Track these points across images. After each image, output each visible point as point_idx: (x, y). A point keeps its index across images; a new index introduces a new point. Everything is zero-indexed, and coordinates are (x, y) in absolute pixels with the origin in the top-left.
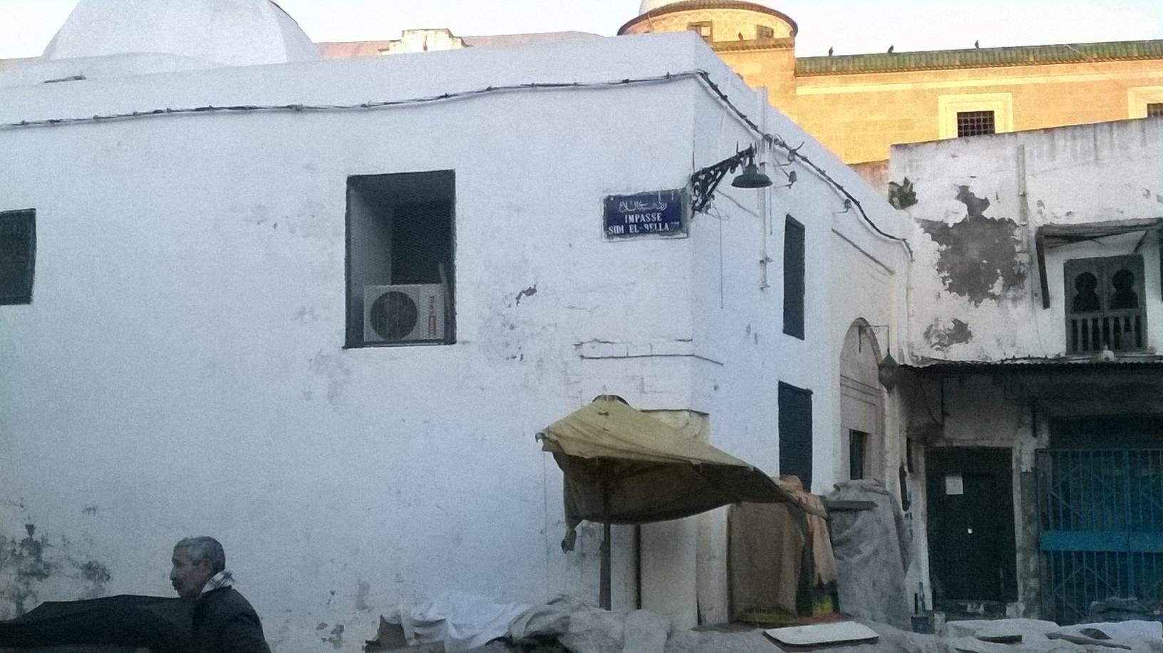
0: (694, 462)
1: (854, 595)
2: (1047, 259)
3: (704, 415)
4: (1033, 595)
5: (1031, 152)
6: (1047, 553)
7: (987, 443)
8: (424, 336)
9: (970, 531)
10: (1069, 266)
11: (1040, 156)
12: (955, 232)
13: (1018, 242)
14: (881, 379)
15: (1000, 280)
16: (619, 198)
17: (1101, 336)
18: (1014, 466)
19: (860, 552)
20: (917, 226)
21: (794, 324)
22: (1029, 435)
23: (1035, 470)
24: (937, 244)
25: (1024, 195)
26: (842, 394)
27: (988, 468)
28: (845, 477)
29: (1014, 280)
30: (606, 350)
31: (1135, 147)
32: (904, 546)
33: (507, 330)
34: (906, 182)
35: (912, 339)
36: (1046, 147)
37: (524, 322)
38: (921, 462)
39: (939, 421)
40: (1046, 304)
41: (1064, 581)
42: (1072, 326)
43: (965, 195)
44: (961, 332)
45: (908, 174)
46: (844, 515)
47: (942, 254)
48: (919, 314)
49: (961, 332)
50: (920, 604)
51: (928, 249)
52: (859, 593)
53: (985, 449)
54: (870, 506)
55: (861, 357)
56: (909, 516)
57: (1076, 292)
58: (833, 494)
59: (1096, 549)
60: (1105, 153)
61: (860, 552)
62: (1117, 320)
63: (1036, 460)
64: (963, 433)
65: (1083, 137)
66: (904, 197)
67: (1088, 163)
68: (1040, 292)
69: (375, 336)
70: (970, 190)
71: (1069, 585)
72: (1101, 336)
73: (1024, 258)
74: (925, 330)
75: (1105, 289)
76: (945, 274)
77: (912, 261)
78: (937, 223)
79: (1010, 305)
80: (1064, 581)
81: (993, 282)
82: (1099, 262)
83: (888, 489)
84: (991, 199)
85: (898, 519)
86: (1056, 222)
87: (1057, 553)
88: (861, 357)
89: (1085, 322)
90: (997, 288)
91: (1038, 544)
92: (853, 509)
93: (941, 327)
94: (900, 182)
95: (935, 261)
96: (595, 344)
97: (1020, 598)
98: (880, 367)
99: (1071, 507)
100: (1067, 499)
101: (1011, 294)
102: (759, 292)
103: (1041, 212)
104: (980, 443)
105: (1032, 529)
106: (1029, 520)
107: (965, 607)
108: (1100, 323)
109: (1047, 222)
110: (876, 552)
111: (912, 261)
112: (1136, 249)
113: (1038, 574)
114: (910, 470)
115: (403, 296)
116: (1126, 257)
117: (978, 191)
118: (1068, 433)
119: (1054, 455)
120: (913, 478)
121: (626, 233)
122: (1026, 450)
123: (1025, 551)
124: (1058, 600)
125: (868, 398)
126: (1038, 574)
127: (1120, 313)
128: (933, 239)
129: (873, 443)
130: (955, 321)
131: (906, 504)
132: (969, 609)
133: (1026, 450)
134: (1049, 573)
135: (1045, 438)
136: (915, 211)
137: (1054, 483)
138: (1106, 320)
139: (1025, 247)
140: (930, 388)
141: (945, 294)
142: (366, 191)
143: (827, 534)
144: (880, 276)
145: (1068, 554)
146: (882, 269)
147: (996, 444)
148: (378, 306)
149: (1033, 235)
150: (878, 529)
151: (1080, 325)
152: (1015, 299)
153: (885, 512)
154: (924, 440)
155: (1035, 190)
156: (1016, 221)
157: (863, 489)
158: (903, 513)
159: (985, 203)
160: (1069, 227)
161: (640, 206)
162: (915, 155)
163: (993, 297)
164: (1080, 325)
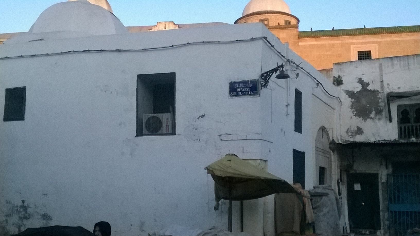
3: (266, 161)
6: (391, 212)
7: (369, 172)
10: (399, 107)
13: (380, 98)
14: (330, 148)
16: (235, 83)
18: (379, 180)
20: (343, 92)
21: (298, 128)
25: (382, 81)
27: (370, 181)
28: (317, 184)
29: (379, 112)
30: (230, 137)
34: (339, 76)
40: (391, 121)
42: (400, 129)
43: (360, 81)
44: (359, 131)
47: (352, 102)
48: (344, 124)
49: (359, 131)
50: (345, 230)
51: (347, 101)
54: (326, 195)
56: (341, 198)
58: (313, 190)
62: (416, 127)
64: (361, 167)
66: (338, 82)
68: (388, 117)
70: (363, 79)
73: (382, 104)
74: (346, 130)
75: (412, 115)
76: (354, 110)
77: (342, 105)
78: (350, 91)
79: (377, 121)
83: (333, 188)
85: (337, 200)
87: (395, 212)
89: (405, 127)
90: (373, 115)
91: (388, 209)
97: (382, 228)
98: (330, 144)
100: (398, 191)
101: (378, 117)
103: (388, 87)
104: (367, 172)
107: (362, 232)
110: (328, 212)
113: (388, 220)
114: (341, 181)
117: (365, 80)
121: (237, 95)
122: (383, 174)
125: (326, 155)
126: (388, 220)
131: (340, 194)
132: (363, 232)
133: (383, 174)
135: (390, 170)
136: (343, 87)
138: (412, 127)
140: (349, 151)
141: (354, 118)
145: (399, 212)
149: (386, 95)
150: (329, 203)
152: (379, 119)
153: (332, 196)
154: (346, 171)
156: (380, 91)
157: (324, 188)
158: (339, 197)
159: (368, 84)
160: (399, 93)
163: (371, 118)
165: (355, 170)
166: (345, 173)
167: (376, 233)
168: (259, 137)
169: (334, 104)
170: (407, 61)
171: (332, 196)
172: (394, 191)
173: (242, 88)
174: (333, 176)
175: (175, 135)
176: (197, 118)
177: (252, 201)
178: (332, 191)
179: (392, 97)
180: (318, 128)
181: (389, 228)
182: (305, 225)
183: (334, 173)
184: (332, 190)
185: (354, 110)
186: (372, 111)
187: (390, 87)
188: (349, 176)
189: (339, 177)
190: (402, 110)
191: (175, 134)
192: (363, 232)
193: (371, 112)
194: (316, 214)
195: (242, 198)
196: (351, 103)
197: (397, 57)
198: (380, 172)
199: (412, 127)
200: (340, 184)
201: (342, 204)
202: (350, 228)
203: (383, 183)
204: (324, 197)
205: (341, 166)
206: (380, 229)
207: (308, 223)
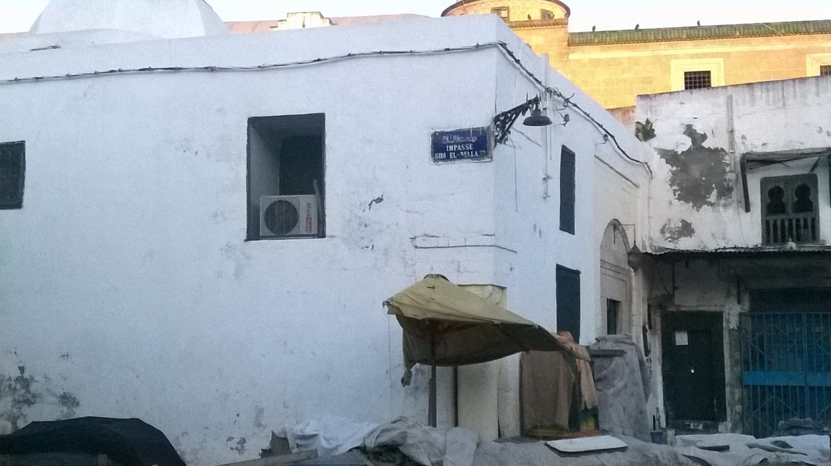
2: (749, 177)
3: (503, 288)
4: (738, 416)
6: (747, 387)
7: (705, 308)
9: (693, 371)
10: (764, 182)
11: (744, 103)
12: (682, 157)
13: (728, 165)
14: (629, 263)
15: (715, 192)
16: (443, 134)
17: (787, 233)
18: (724, 325)
21: (567, 223)
23: (740, 328)
25: (732, 132)
27: (706, 326)
28: (604, 333)
29: (725, 192)
30: (434, 242)
31: (811, 97)
32: (646, 382)
33: (363, 227)
34: (648, 122)
36: (748, 97)
40: (748, 209)
43: (690, 131)
44: (687, 229)
45: (649, 116)
47: (674, 173)
48: (656, 216)
49: (687, 229)
50: (657, 423)
51: (663, 170)
53: (700, 312)
54: (621, 353)
55: (614, 247)
56: (650, 361)
57: (769, 201)
58: (595, 344)
60: (790, 101)
61: (614, 386)
62: (798, 221)
64: (689, 301)
66: (646, 132)
67: (778, 108)
71: (763, 409)
73: (731, 176)
74: (660, 227)
75: (789, 198)
76: (676, 187)
79: (721, 209)
82: (787, 180)
84: (709, 134)
85: (641, 363)
86: (755, 150)
87: (755, 387)
88: (614, 247)
90: (713, 198)
91: (740, 380)
93: (672, 226)
94: (644, 122)
95: (668, 178)
96: (427, 238)
97: (728, 419)
98: (629, 254)
101: (722, 202)
103: (743, 143)
104: (700, 309)
105: (737, 369)
106: (734, 364)
108: (787, 223)
110: (625, 386)
111: (652, 178)
112: (813, 169)
114: (650, 328)
116: (804, 175)
117: (699, 128)
119: (753, 317)
121: (448, 158)
122: (733, 313)
125: (620, 276)
127: (801, 216)
129: (624, 307)
130: (683, 221)
131: (647, 352)
132: (692, 427)
133: (733, 313)
134: (749, 399)
135: (746, 305)
136: (654, 142)
137: (753, 336)
138: (790, 220)
139: (733, 168)
140: (665, 270)
142: (261, 128)
143: (591, 373)
145: (763, 387)
148: (270, 210)
149: (738, 159)
150: (627, 371)
153: (632, 357)
154: (661, 306)
155: (740, 128)
158: (645, 358)
159: (704, 137)
161: (458, 139)
165: (679, 306)
168: (490, 241)
170: (780, 91)
183: (637, 311)
185: (676, 187)
189: (647, 321)
190: (771, 186)
191: (324, 236)
193: (709, 191)
196: (670, 175)
197: (761, 83)
198: (726, 310)
199: (790, 220)
200: (648, 334)
202: (667, 418)
203: (731, 331)
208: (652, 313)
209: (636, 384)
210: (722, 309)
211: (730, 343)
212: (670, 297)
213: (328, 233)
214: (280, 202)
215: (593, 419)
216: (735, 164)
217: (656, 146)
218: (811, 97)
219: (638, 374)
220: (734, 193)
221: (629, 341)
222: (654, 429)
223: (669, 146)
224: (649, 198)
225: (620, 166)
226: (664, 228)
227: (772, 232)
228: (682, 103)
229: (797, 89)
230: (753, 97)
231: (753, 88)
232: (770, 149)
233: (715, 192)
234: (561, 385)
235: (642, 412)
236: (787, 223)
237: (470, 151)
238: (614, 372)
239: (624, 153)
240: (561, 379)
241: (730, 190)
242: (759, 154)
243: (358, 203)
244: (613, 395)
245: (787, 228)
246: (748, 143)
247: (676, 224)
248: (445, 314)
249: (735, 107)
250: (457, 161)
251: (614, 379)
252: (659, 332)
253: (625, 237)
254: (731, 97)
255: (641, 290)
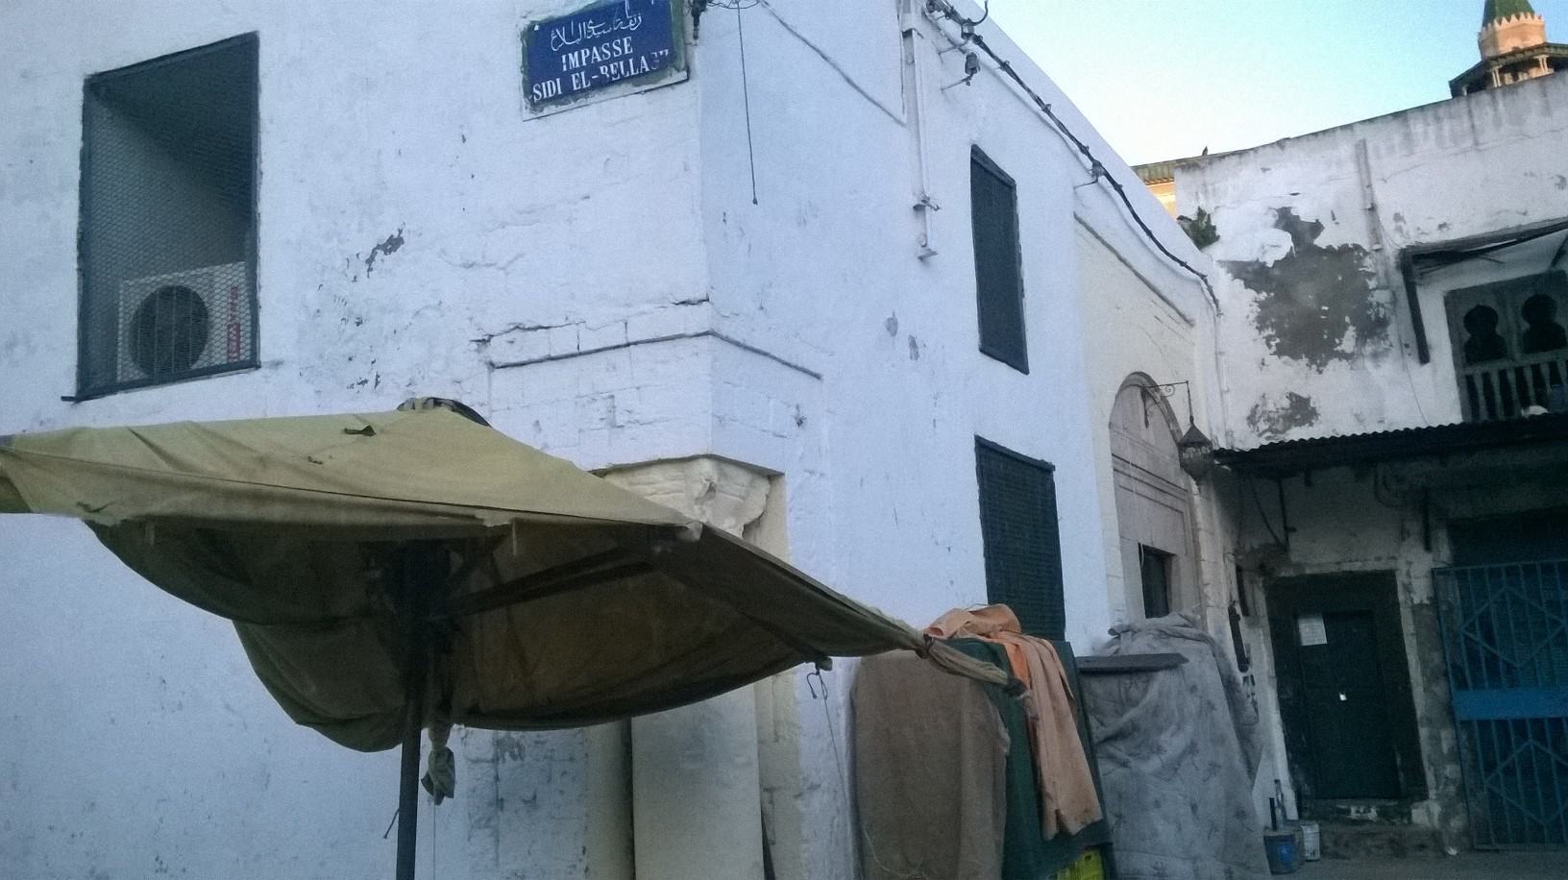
0: (490, 521)
1: (1155, 834)
2: (1420, 293)
3: (772, 477)
4: (1452, 789)
5: (1376, 149)
6: (1467, 724)
7: (1357, 566)
8: (220, 357)
9: (1343, 697)
10: (1452, 300)
11: (1391, 149)
12: (1277, 272)
13: (1370, 275)
14: (1185, 466)
15: (1351, 332)
16: (549, 25)
17: (1515, 396)
18: (1401, 597)
19: (1159, 750)
20: (1222, 271)
21: (1003, 334)
22: (1420, 549)
23: (1435, 600)
24: (1252, 293)
25: (1373, 209)
26: (1118, 487)
27: (1361, 603)
28: (1136, 615)
29: (1372, 328)
30: (537, 345)
31: (1534, 120)
32: (1246, 733)
33: (350, 328)
34: (1201, 213)
35: (1231, 424)
36: (1397, 139)
37: (383, 310)
38: (1260, 600)
39: (1282, 538)
40: (1424, 357)
41: (1501, 766)
42: (1468, 387)
43: (1286, 220)
44: (1301, 409)
45: (1202, 203)
46: (1126, 681)
47: (1262, 305)
48: (1237, 386)
49: (1301, 409)
50: (1279, 812)
51: (1241, 302)
52: (1165, 831)
53: (1352, 576)
54: (1173, 663)
55: (1148, 435)
56: (1250, 680)
57: (1466, 336)
58: (1110, 644)
59: (1528, 715)
60: (1488, 136)
61: (1159, 750)
62: (1536, 368)
63: (1435, 587)
64: (1319, 554)
65: (1451, 117)
66: (1202, 233)
67: (1465, 151)
68: (1414, 345)
69: (136, 374)
70: (1294, 213)
71: (1509, 771)
72: (1515, 396)
73: (1382, 297)
74: (1247, 413)
75: (1511, 325)
76: (1269, 332)
77: (1219, 314)
78: (1249, 264)
79: (1368, 364)
80: (1501, 766)
81: (1341, 336)
82: (1497, 289)
83: (1211, 633)
84: (1325, 221)
85: (1229, 684)
86: (1426, 240)
87: (1484, 725)
88: (1148, 435)
89: (1486, 376)
90: (1348, 342)
91: (1450, 710)
92: (1140, 669)
93: (1271, 407)
94: (1192, 214)
95: (1252, 317)
96: (517, 335)
97: (1432, 793)
98: (1182, 446)
99: (1498, 653)
100: (1489, 637)
101: (1369, 349)
102: (917, 263)
103: (1399, 229)
104: (1347, 567)
105: (1440, 689)
106: (1431, 678)
107: (1348, 812)
108: (1511, 376)
109: (1412, 242)
110: (1192, 749)
111: (1219, 314)
112: (1555, 262)
113: (1456, 756)
114: (1246, 612)
115: (184, 293)
116: (1537, 277)
117: (1305, 212)
118: (1476, 542)
119: (1461, 576)
120: (1251, 625)
121: (568, 95)
122: (1416, 571)
123: (1430, 721)
124: (1493, 796)
125: (1169, 500)
126: (1456, 756)
127: (1543, 358)
128: (1247, 286)
129: (1182, 569)
130: (1291, 396)
131: (1244, 663)
132: (1354, 815)
133: (1416, 571)
134: (1473, 751)
135: (1445, 553)
136: (1217, 251)
137: (1466, 616)
138: (1519, 371)
139: (1383, 282)
140: (1269, 482)
141: (1274, 361)
142: (111, 94)
143: (1071, 724)
144: (1173, 325)
145: (1502, 723)
146: (1172, 312)
147: (1372, 565)
148: (146, 315)
149: (1392, 262)
150: (1192, 704)
151: (1479, 384)
152: (1375, 356)
153: (1203, 670)
154: (1262, 569)
155: (1388, 200)
156: (1366, 247)
157: (1163, 634)
158: (1240, 676)
159: (1316, 228)
160: (1447, 244)
161: (591, 29)
162: (1212, 175)
163: (1344, 356)
164: (1479, 384)
165: (1298, 565)
166: (1260, 580)
167: (1409, 815)
168: (696, 319)
169: (1191, 301)
170: (1466, 118)
171: (1203, 670)
172: (1467, 638)
173: (588, 44)
174: (1208, 590)
175: (258, 367)
176: (364, 257)
177: (685, 712)
178: (1204, 646)
179: (1420, 262)
180: (1121, 379)
181: (1462, 792)
182: (1033, 846)
183: (1211, 574)
184: (1203, 638)
185: (1269, 332)
186: (1345, 327)
187: (1405, 228)
188: (1277, 591)
189: (1236, 596)
190: (1463, 310)
191: (253, 364)
192: (1354, 815)
193: (1339, 330)
194: (1124, 764)
195: (609, 699)
196: (1256, 308)
197: (1422, 108)
198: (1401, 566)
199: (1519, 371)
200: (1242, 624)
201: (1254, 703)
202: (1300, 797)
203: (1416, 610)
204: (1161, 675)
205: (1236, 553)
206: (1424, 797)
207: (1063, 832)
208: (1246, 583)
209: (1220, 740)
210: (1391, 565)
211: (1417, 634)
212: (1283, 548)
213: (264, 356)
214: (167, 293)
215: (1095, 857)
216: (1386, 274)
217: (1222, 258)
218: (1534, 120)
219: (1223, 713)
220: (1391, 329)
221: (1194, 631)
222: (1275, 827)
223: (1245, 254)
224: (1218, 354)
225: (1144, 264)
226: (1254, 412)
227: (1482, 398)
228: (1264, 170)
229: (1501, 107)
230: (1408, 137)
231: (1406, 120)
232: (1457, 233)
233: (1351, 332)
234: (969, 764)
235: (1241, 814)
236: (1511, 376)
237: (625, 58)
238: (1156, 712)
239: (1149, 233)
240: (969, 742)
241: (1382, 323)
242: (1434, 246)
243: (339, 262)
244: (1158, 774)
245: (1514, 387)
246: (1408, 227)
247: (1279, 403)
248: (232, 495)
249: (1372, 162)
250: (597, 97)
251: (1160, 730)
252: (1265, 621)
253: (1170, 418)
254: (1364, 142)
255: (1218, 531)
